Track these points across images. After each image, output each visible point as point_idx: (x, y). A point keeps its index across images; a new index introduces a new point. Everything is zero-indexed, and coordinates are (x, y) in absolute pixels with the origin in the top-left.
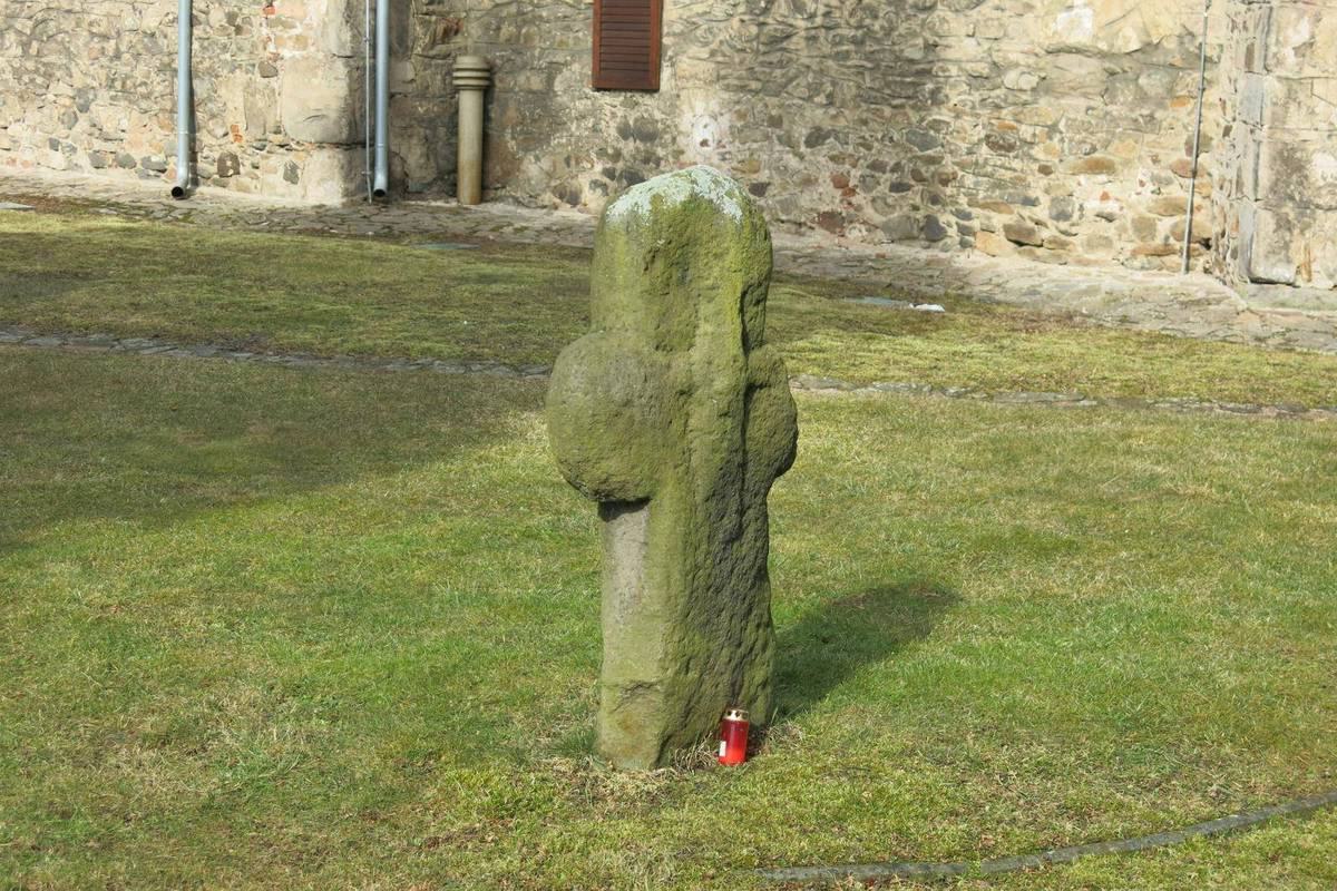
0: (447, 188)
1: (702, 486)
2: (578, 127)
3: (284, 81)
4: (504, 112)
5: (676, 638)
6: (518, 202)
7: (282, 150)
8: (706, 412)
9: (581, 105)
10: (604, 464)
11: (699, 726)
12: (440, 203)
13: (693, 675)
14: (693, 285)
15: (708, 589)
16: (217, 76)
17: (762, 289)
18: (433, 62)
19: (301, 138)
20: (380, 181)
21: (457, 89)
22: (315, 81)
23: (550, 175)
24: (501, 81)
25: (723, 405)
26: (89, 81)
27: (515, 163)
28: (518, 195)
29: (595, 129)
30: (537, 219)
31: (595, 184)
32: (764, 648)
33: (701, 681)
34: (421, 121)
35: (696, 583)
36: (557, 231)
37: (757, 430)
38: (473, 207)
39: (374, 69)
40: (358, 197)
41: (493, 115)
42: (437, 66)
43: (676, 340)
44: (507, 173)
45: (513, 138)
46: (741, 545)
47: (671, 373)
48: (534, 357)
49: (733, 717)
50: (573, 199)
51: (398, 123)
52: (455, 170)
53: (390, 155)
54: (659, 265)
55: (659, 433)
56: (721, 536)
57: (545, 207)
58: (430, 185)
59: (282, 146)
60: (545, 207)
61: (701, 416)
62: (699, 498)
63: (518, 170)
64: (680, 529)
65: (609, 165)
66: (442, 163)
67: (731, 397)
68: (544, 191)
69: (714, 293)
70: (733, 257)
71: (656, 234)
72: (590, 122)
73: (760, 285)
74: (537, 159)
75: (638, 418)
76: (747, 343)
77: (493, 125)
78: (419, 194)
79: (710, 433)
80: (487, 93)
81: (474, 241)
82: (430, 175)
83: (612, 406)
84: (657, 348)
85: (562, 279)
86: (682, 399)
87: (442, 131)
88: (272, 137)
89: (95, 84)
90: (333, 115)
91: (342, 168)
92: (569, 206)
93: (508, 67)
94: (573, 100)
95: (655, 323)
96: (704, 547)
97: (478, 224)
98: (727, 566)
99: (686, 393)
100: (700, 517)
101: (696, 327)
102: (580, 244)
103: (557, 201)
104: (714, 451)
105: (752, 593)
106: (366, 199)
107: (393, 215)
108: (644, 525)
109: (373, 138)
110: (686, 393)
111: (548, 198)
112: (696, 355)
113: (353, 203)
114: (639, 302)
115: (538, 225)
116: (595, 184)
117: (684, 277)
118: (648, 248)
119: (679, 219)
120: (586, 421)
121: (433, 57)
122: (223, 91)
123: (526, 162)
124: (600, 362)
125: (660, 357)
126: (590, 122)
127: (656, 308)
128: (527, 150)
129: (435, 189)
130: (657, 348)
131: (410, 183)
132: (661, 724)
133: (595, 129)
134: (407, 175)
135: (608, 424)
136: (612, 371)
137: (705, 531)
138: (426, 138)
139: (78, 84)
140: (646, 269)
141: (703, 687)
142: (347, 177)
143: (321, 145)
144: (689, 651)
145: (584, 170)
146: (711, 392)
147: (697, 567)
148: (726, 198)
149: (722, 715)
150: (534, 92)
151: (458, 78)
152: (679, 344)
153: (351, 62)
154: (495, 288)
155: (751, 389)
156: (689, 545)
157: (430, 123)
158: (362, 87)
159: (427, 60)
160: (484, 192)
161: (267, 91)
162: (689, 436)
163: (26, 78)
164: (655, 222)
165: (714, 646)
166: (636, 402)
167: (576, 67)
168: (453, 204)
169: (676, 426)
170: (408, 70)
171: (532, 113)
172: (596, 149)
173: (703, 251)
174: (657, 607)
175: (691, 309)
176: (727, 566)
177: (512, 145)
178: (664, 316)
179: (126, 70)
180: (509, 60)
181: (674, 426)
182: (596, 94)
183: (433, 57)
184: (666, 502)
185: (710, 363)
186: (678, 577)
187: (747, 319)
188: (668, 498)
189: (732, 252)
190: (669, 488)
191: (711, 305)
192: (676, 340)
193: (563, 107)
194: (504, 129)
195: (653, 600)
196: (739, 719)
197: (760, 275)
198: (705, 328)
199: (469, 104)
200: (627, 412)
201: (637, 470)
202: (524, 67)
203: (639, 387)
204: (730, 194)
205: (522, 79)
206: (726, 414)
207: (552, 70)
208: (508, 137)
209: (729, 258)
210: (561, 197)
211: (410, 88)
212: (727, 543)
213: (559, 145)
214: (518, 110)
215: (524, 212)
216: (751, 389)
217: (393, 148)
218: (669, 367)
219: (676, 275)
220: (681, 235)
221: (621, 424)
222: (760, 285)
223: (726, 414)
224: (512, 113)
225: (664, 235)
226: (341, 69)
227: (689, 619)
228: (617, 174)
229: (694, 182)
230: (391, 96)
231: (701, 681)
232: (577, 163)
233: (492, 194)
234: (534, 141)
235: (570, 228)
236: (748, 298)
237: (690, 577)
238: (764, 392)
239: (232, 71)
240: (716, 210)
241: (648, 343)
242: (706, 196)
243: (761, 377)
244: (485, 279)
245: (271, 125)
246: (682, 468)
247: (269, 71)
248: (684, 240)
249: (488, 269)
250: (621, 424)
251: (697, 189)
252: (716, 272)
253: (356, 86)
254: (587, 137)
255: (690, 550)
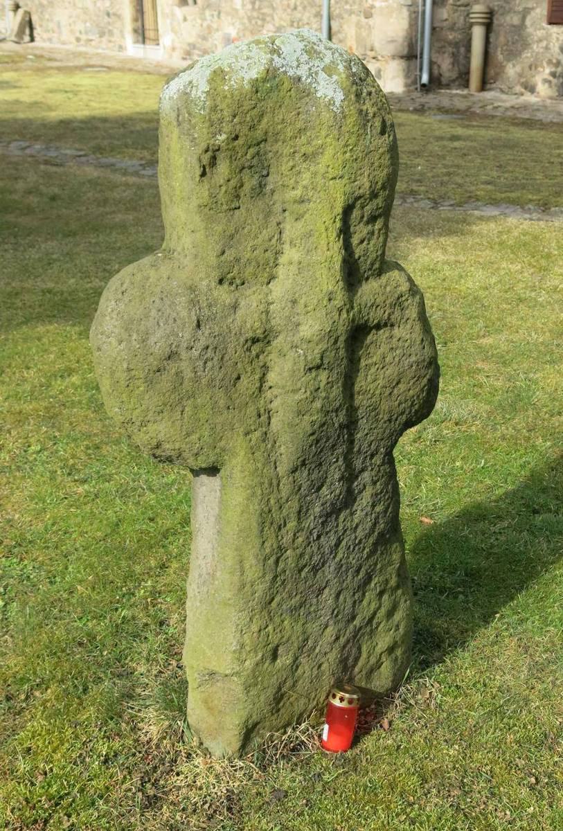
0: (463, 83)
1: (286, 453)
2: (537, 47)
3: (376, 21)
4: (497, 39)
5: (255, 628)
6: (502, 91)
7: (374, 61)
8: (288, 366)
9: (540, 33)
10: (152, 428)
11: (300, 705)
12: (458, 92)
13: (284, 660)
14: (276, 197)
15: (300, 571)
16: (342, 18)
17: (379, 201)
18: (460, 8)
19: (384, 53)
20: (425, 78)
21: (472, 25)
22: (392, 20)
23: (520, 75)
24: (497, 19)
25: (314, 356)
26: (282, 23)
27: (502, 67)
28: (502, 87)
29: (547, 48)
30: (509, 101)
31: (545, 81)
32: (390, 614)
33: (295, 665)
34: (450, 43)
35: (281, 565)
36: (518, 108)
37: (371, 381)
38: (476, 94)
39: (424, 12)
40: (412, 88)
41: (491, 40)
42: (461, 11)
43: (250, 270)
44: (497, 74)
45: (502, 54)
46: (352, 514)
47: (240, 313)
48: (450, 194)
49: (336, 702)
50: (532, 89)
51: (437, 45)
52: (468, 73)
53: (431, 63)
54: (223, 168)
55: (220, 394)
56: (317, 509)
57: (516, 94)
58: (454, 81)
59: (374, 58)
60: (516, 94)
61: (284, 368)
62: (283, 469)
63: (504, 72)
64: (255, 507)
65: (553, 69)
66: (462, 68)
67: (323, 346)
68: (516, 85)
69: (303, 207)
70: (330, 158)
71: (214, 125)
72: (544, 44)
73: (374, 195)
74: (514, 66)
75: (188, 374)
76: (352, 274)
77: (491, 46)
78: (448, 86)
79: (295, 391)
80: (488, 27)
81: (465, 115)
82: (454, 75)
83: (151, 359)
84: (221, 282)
85: (499, 139)
86: (255, 349)
87: (462, 50)
88: (369, 53)
89: (285, 24)
90: (400, 40)
91: (404, 70)
92: (529, 94)
93: (500, 12)
94: (535, 31)
95: (218, 248)
96: (292, 525)
97: (474, 103)
98: (328, 541)
99: (261, 340)
100: (285, 489)
101: (278, 253)
102: (527, 117)
103: (523, 90)
104: (300, 413)
105: (371, 561)
106: (416, 89)
107: (431, 99)
108: (218, 493)
109: (422, 54)
110: (261, 340)
111: (518, 89)
112: (278, 290)
113: (409, 91)
114: (197, 218)
115: (508, 105)
116: (545, 81)
117: (261, 186)
118: (203, 146)
119: (247, 105)
120: (122, 376)
121: (459, 6)
122: (345, 27)
123: (508, 67)
124: (142, 299)
125: (224, 295)
126: (544, 44)
127: (219, 228)
128: (509, 61)
129: (457, 83)
130: (221, 282)
131: (443, 79)
132: (244, 714)
133: (547, 48)
134: (441, 75)
135: (150, 382)
136: (153, 313)
137: (294, 505)
138: (453, 54)
139: (277, 25)
140: (203, 174)
141: (300, 671)
142: (407, 76)
143: (393, 57)
144: (274, 639)
145: (539, 72)
146: (296, 339)
147: (281, 549)
148: (322, 75)
149: (327, 697)
150: (514, 26)
151: (472, 18)
152: (255, 275)
153: (412, 9)
154: (456, 144)
155: (358, 334)
156: (268, 521)
157: (456, 45)
158: (417, 23)
159: (455, 8)
160: (484, 85)
161: (367, 27)
162: (269, 394)
163: (253, 22)
164: (214, 109)
165: (313, 628)
166: (184, 355)
167: (538, 10)
168: (465, 92)
169: (247, 384)
170: (444, 13)
171: (513, 39)
172: (547, 60)
173: (287, 150)
174: (228, 595)
175: (272, 229)
176: (328, 541)
177: (500, 57)
178: (230, 238)
179: (299, 15)
180: (502, 7)
181: (244, 381)
182: (549, 26)
183: (459, 6)
184: (237, 474)
185: (294, 302)
186: (254, 562)
187: (355, 240)
188: (238, 465)
189: (329, 152)
190: (239, 459)
191: (300, 225)
192: (250, 270)
193: (530, 35)
194: (497, 48)
195: (225, 583)
196: (344, 705)
197: (373, 183)
198: (291, 254)
199: (478, 33)
200: (172, 367)
201: (194, 437)
202: (509, 12)
203: (187, 336)
204: (329, 70)
205: (508, 18)
206: (318, 367)
207: (525, 13)
208: (499, 53)
209: (325, 159)
210: (526, 88)
211: (445, 24)
212: (328, 515)
213: (527, 57)
214: (505, 37)
215: (504, 97)
216: (358, 334)
217: (434, 60)
218: (235, 307)
219: (250, 182)
220: (252, 128)
221: (165, 382)
222: (374, 195)
223: (318, 367)
224: (502, 39)
225: (227, 128)
226: (405, 13)
227: (274, 604)
228: (557, 75)
229: (276, 51)
230: (433, 29)
231: (295, 665)
232: (536, 68)
233: (488, 86)
234: (513, 54)
235: (525, 107)
236: (356, 213)
237: (271, 561)
238: (383, 334)
239: (350, 15)
240: (301, 90)
241: (208, 276)
242: (291, 73)
243: (375, 316)
244: (454, 138)
245: (369, 47)
246: (258, 434)
247: (368, 15)
248: (259, 134)
249: (460, 131)
250: (165, 382)
251: (278, 61)
252: (306, 178)
253: (413, 22)
254: (542, 53)
255: (269, 532)
